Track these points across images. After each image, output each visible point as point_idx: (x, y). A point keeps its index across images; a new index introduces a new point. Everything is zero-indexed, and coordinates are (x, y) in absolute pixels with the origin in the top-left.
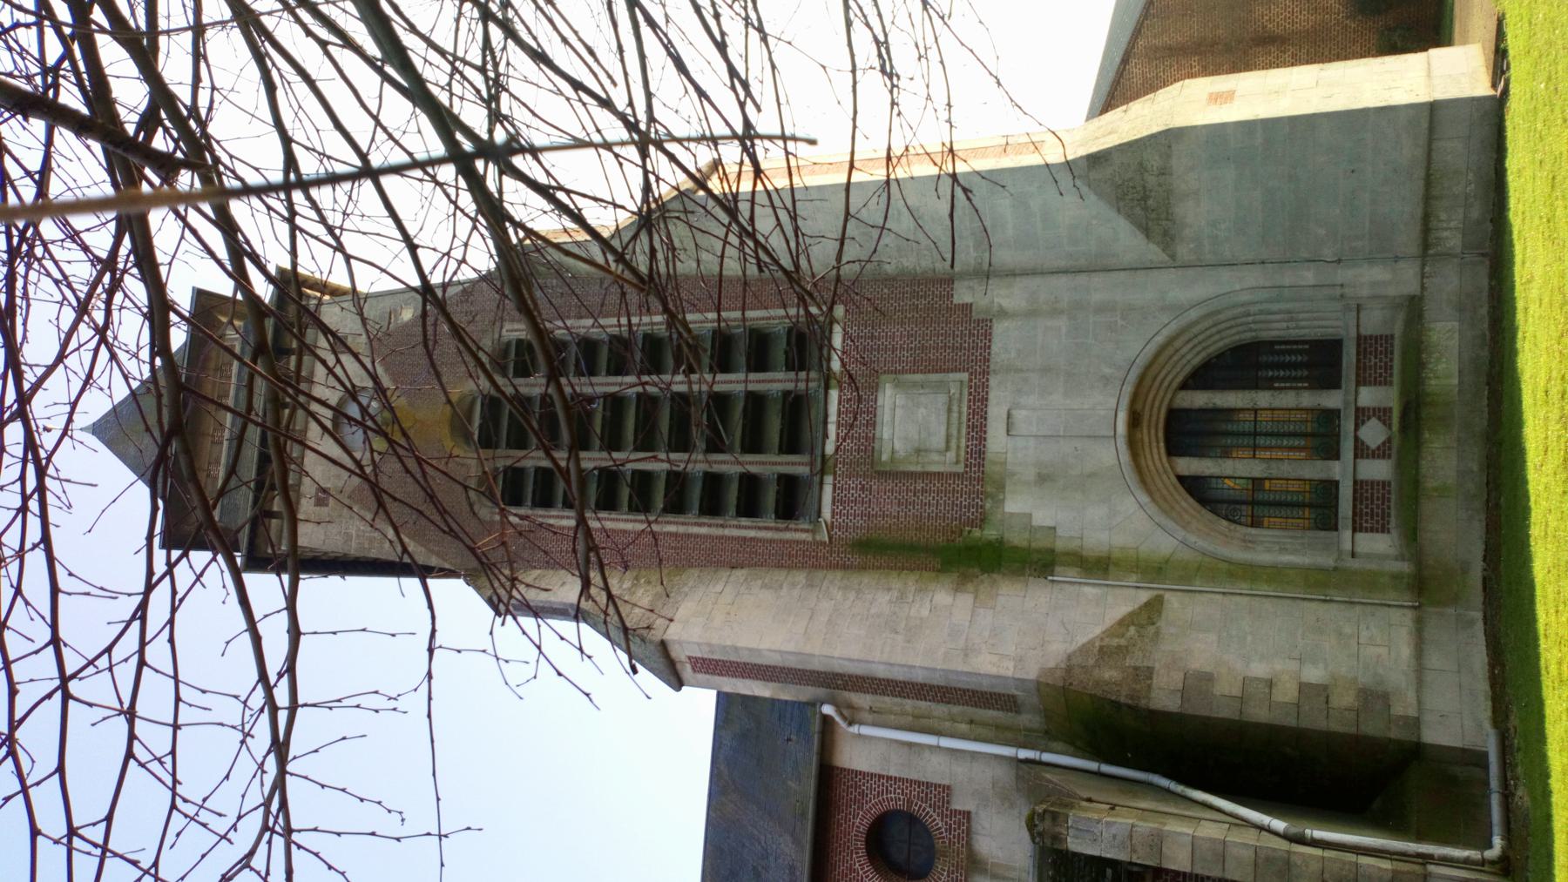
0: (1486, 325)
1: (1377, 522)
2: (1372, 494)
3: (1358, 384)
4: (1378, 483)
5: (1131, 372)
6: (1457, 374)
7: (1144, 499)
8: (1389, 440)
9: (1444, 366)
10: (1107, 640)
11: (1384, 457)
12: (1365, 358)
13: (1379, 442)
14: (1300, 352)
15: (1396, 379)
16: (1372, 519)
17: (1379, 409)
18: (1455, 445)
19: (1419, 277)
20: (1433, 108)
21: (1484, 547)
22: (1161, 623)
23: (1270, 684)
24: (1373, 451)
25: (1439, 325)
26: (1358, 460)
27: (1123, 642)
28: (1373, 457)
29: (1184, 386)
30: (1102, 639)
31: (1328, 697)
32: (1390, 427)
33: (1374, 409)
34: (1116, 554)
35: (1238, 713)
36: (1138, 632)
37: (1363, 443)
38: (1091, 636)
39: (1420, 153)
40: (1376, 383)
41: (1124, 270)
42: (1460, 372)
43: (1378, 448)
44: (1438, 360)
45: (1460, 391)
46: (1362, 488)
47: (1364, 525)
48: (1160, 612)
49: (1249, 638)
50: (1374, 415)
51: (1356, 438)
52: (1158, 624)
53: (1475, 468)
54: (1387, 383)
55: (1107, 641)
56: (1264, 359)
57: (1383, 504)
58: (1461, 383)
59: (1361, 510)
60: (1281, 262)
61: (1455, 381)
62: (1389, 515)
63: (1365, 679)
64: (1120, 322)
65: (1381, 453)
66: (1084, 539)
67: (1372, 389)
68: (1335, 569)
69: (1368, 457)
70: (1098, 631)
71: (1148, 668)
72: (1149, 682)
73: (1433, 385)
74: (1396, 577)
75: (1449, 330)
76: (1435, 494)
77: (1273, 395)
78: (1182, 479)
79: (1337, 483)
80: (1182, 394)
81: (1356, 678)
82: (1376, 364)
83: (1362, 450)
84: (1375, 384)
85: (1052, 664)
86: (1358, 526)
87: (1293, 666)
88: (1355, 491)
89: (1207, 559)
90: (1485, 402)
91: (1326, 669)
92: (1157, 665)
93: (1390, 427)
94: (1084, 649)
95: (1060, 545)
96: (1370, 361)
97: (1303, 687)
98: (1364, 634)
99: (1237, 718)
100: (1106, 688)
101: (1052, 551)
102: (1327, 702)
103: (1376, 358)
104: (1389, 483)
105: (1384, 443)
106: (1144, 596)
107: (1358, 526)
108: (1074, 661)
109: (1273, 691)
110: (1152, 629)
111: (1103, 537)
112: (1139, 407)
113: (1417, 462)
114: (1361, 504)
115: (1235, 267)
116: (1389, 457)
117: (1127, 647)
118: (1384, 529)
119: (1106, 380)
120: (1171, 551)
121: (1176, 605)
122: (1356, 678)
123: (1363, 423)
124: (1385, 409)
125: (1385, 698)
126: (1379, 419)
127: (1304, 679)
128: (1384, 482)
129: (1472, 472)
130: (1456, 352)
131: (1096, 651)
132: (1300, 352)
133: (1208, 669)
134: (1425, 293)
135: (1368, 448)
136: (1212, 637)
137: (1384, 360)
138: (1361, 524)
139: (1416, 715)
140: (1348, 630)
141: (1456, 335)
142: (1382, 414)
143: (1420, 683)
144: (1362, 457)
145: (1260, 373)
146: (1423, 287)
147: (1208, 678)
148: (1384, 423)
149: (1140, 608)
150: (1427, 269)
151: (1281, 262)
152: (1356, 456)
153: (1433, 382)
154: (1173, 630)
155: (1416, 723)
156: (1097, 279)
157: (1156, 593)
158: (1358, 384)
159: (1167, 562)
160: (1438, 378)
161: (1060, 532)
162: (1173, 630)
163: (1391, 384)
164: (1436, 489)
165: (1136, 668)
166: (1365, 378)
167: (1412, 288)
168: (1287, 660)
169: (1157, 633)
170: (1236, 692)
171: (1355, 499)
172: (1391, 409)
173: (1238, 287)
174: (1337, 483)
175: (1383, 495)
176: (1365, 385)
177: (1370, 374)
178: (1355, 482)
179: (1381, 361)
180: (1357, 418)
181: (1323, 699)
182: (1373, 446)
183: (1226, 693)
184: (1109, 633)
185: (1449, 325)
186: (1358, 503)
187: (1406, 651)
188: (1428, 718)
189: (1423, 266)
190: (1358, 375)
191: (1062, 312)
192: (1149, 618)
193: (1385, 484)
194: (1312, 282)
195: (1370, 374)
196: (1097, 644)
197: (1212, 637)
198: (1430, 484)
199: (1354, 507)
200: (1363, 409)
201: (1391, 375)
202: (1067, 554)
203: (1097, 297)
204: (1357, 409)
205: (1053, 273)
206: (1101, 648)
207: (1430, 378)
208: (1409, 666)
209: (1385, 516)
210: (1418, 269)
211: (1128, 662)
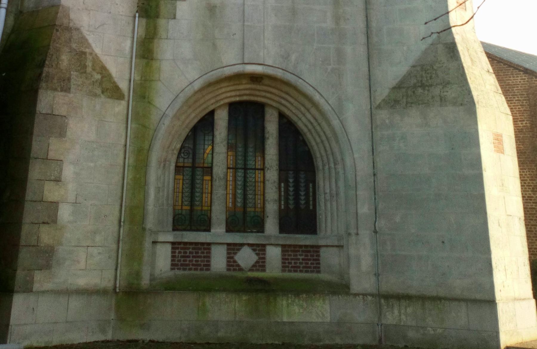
0: (327, 342)
1: (179, 261)
2: (200, 257)
3: (283, 246)
4: (209, 261)
5: (293, 76)
6: (290, 321)
7: (197, 85)
8: (241, 269)
9: (297, 311)
10: (91, 58)
11: (228, 265)
12: (303, 251)
13: (240, 262)
14: (307, 203)
15: (287, 275)
16: (182, 257)
17: (264, 262)
18: (237, 319)
19: (364, 292)
20: (491, 303)
21: (161, 340)
22: (103, 98)
23: (58, 180)
24: (232, 258)
25: (327, 307)
26: (226, 246)
27: (89, 70)
28: (228, 258)
29: (282, 116)
30: (91, 54)
31: (48, 223)
32: (251, 270)
33: (264, 258)
34: (155, 64)
35: (35, 156)
36: (97, 81)
37: (239, 250)
38: (93, 45)
39: (457, 293)
40: (284, 259)
41: (369, 71)
42: (292, 323)
43: (235, 261)
44: (302, 306)
45: (278, 322)
46: (205, 249)
47: (177, 251)
48: (111, 97)
49: (92, 165)
50: (260, 258)
51: (242, 245)
52: (102, 96)
53: (220, 334)
54: (284, 268)
55: (89, 57)
56: (302, 176)
57: (193, 265)
58: (284, 323)
59: (189, 249)
60: (375, 188)
61: (285, 319)
62: (184, 269)
63: (61, 251)
64: (330, 68)
65: (232, 264)
66: (166, 41)
67: (279, 257)
68: (144, 229)
69: (228, 253)
70: (98, 51)
71: (70, 89)
72: (59, 89)
73: (283, 302)
74: (138, 275)
75: (323, 315)
76: (200, 304)
77: (275, 182)
78: (212, 113)
79: (209, 230)
80: (276, 114)
81: (61, 244)
82: (299, 259)
83: (233, 249)
84: (283, 259)
85: (72, 16)
86: (177, 246)
87: (71, 198)
88: (203, 244)
89: (151, 132)
90: (270, 342)
91: (69, 222)
92: (71, 95)
93: (251, 270)
94: (83, 41)
95: (162, 22)
96: (301, 255)
97: (54, 205)
98: (95, 251)
99: (32, 155)
100: (54, 57)
101: (157, 16)
102: (44, 223)
103: (303, 259)
104: (208, 270)
105: (238, 265)
106: (123, 85)
107: (177, 246)
108: (74, 33)
109: (52, 182)
110: (98, 91)
111: (168, 55)
112: (266, 81)
113: (224, 290)
114: (193, 249)
115: (371, 153)
116: (228, 270)
117: (85, 72)
118: (174, 266)
119: (286, 57)
120: (158, 106)
121: (117, 110)
122: (61, 244)
123: (254, 250)
124: (264, 266)
125: (47, 266)
126: (257, 262)
127: (61, 206)
128: (209, 265)
129: (217, 332)
130: (308, 319)
131: (83, 49)
132: (307, 203)
133: (68, 133)
134: (351, 297)
135: (235, 254)
136: (93, 136)
137: (301, 266)
138: (178, 248)
139: (34, 290)
140: (98, 238)
141: (320, 320)
142: (260, 265)
143: (58, 293)
144: (228, 249)
145: (291, 172)
146: (356, 295)
147: (62, 133)
148: (254, 266)
149: (114, 82)
150: (370, 298)
151: (375, 188)
152: (228, 244)
153: (284, 302)
154: (98, 107)
155: (28, 289)
156: (362, 50)
157: (126, 94)
158: (283, 246)
159: (149, 103)
160: (288, 306)
161: (172, 22)
162: (98, 107)
163: (283, 271)
164: (204, 304)
165: (69, 79)
166: (288, 251)
167: (355, 287)
168: (75, 193)
169: (96, 95)
170: (51, 155)
171: (196, 244)
172: (264, 270)
173: (356, 156)
174: (209, 230)
175: (200, 265)
176: (283, 251)
177: (290, 255)
178: (209, 244)
179: (301, 263)
180: (258, 245)
181: (46, 219)
182: (236, 258)
183: (50, 147)
184: (96, 60)
185: (328, 315)
186: (193, 246)
187: (82, 282)
188: (32, 298)
189: (372, 295)
190: (290, 246)
191: (337, 23)
192: (107, 89)
193: (208, 266)
194: (360, 211)
195: (290, 255)
196: (87, 50)
197: (93, 136)
198: (208, 300)
199: (191, 243)
200: (264, 250)
201: (290, 271)
202: (155, 28)
203: (348, 49)
204: (264, 246)
205: (367, 17)
206: (85, 53)
207: (288, 300)
208: (71, 284)
209: (184, 266)
210: (369, 291)
211: (74, 74)
